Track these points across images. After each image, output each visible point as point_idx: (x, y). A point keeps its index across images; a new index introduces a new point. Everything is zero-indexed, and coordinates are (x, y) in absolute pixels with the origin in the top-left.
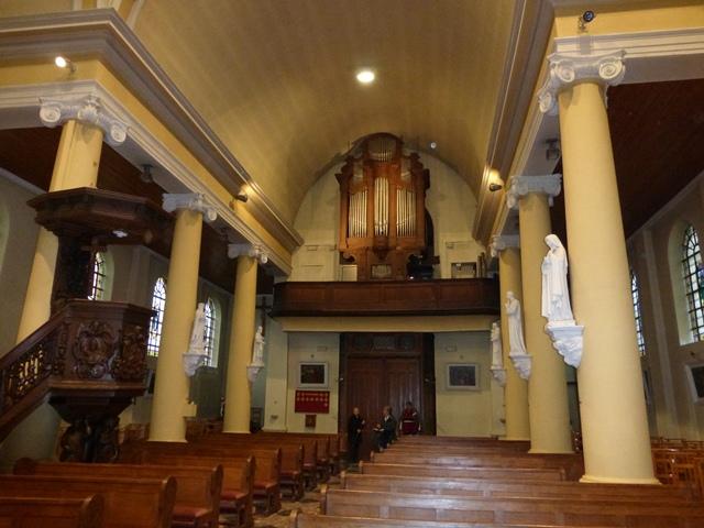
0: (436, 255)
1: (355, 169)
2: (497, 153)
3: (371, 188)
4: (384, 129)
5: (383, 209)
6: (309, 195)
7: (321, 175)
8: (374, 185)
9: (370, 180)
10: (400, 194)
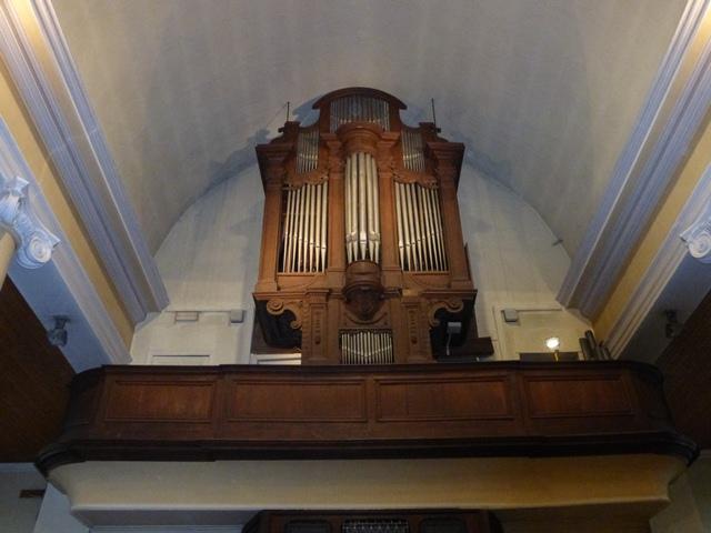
0: (481, 335)
4: (366, 80)
5: (366, 216)
7: (223, 177)
8: (343, 170)
9: (335, 161)
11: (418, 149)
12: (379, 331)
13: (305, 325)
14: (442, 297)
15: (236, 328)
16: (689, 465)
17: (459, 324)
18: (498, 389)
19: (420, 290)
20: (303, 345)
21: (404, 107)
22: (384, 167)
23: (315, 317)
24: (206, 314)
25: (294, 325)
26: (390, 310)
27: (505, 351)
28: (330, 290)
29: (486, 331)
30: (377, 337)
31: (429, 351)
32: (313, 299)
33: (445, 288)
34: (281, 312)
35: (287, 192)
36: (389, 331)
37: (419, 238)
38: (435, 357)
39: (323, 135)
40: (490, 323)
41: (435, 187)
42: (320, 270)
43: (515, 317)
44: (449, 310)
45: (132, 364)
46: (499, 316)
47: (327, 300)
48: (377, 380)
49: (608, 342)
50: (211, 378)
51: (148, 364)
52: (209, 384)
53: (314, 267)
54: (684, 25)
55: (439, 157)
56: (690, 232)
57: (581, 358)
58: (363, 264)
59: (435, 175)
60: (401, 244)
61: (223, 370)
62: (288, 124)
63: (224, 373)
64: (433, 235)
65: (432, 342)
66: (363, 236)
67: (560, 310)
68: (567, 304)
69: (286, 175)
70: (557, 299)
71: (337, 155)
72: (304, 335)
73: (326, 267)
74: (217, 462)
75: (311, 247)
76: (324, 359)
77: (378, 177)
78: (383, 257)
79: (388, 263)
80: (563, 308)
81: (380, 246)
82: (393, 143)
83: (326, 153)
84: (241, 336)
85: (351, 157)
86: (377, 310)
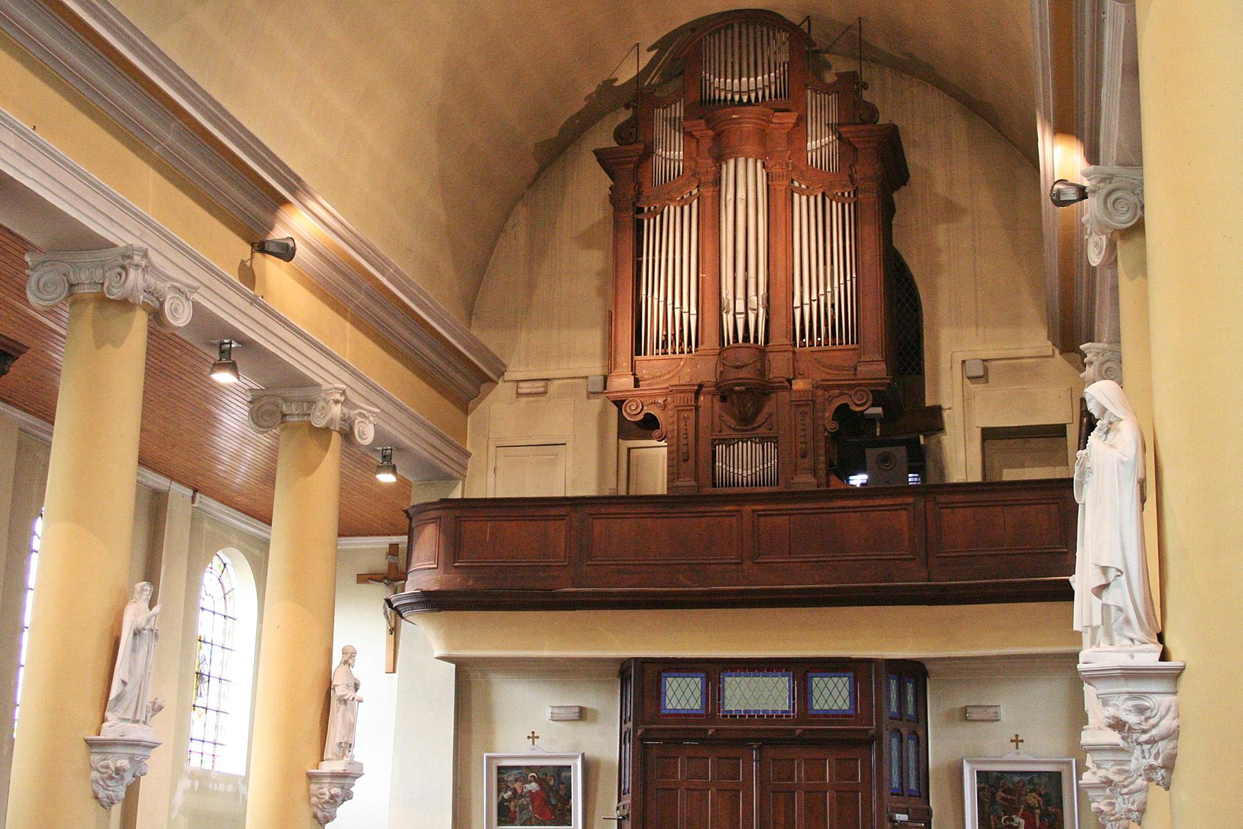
0: (929, 402)
3: (708, 192)
6: (521, 212)
7: (554, 154)
8: (717, 182)
9: (707, 164)
12: (763, 440)
22: (777, 170)
23: (682, 425)
29: (936, 393)
30: (759, 447)
34: (641, 417)
36: (775, 440)
48: (754, 511)
50: (563, 511)
60: (797, 303)
67: (1053, 356)
69: (639, 194)
73: (697, 346)
75: (677, 312)
76: (693, 483)
86: (756, 414)
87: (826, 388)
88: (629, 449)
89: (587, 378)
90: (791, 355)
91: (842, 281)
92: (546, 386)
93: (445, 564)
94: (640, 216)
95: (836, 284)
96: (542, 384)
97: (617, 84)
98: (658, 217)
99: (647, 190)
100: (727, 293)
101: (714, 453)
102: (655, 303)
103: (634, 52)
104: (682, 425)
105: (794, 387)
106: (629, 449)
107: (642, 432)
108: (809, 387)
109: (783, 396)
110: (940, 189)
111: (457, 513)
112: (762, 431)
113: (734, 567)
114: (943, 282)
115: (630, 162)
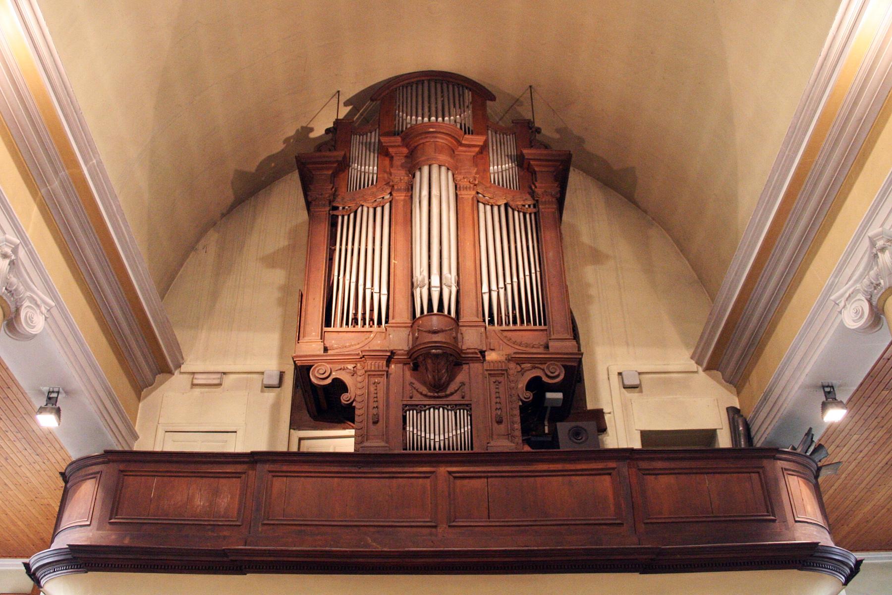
0: (590, 406)
1: (355, 151)
2: (532, 551)
3: (400, 197)
4: (443, 59)
5: (438, 246)
6: (213, 237)
8: (410, 188)
9: (400, 176)
10: (487, 217)
11: (510, 157)
12: (455, 407)
13: (358, 399)
14: (536, 362)
15: (271, 395)
16: (846, 584)
17: (559, 395)
18: (605, 484)
19: (510, 351)
20: (356, 418)
21: (493, 98)
22: (464, 183)
23: (372, 389)
24: (232, 377)
25: (344, 398)
26: (469, 377)
27: (622, 435)
28: (393, 353)
29: (596, 399)
30: (451, 414)
31: (518, 433)
32: (370, 364)
33: (541, 350)
34: (329, 381)
35: (337, 216)
36: (468, 407)
37: (508, 280)
38: (526, 441)
39: (383, 139)
40: (604, 392)
41: (532, 209)
42: (380, 323)
43: (637, 382)
44: (545, 379)
45: (137, 447)
46: (615, 379)
47: (388, 366)
48: (450, 473)
49: (757, 411)
50: (240, 468)
51: (158, 449)
52: (237, 475)
53: (372, 319)
54: (834, 38)
55: (536, 169)
56: (842, 296)
57: (724, 441)
58: (435, 318)
59: (532, 194)
60: (485, 289)
61: (254, 458)
62: (337, 122)
63: (256, 462)
64: (528, 275)
65: (523, 421)
66: (435, 281)
67: (696, 372)
68: (705, 364)
69: (335, 195)
70: (692, 358)
71: (402, 166)
72: (357, 412)
73: (387, 322)
74: (248, 575)
75: (368, 293)
76: (383, 444)
77: (456, 195)
78: (461, 306)
79: (469, 314)
80: (700, 369)
81: (458, 292)
82: (477, 149)
83: (387, 162)
84: (276, 407)
85: (420, 169)
86: (451, 379)
87: (519, 361)
88: (300, 439)
89: (262, 373)
90: (483, 329)
91: (527, 273)
92: (221, 378)
93: (99, 523)
94: (335, 213)
95: (521, 276)
96: (219, 376)
97: (312, 135)
98: (352, 216)
99: (342, 190)
100: (420, 273)
101: (404, 418)
102: (345, 282)
103: (335, 100)
104: (372, 389)
105: (488, 358)
106: (300, 439)
107: (313, 423)
108: (503, 358)
109: (476, 367)
110: (585, 239)
111: (122, 467)
112: (456, 398)
113: (427, 530)
114: (595, 310)
115: (328, 169)
